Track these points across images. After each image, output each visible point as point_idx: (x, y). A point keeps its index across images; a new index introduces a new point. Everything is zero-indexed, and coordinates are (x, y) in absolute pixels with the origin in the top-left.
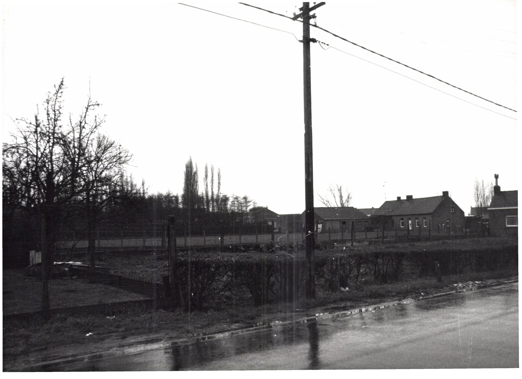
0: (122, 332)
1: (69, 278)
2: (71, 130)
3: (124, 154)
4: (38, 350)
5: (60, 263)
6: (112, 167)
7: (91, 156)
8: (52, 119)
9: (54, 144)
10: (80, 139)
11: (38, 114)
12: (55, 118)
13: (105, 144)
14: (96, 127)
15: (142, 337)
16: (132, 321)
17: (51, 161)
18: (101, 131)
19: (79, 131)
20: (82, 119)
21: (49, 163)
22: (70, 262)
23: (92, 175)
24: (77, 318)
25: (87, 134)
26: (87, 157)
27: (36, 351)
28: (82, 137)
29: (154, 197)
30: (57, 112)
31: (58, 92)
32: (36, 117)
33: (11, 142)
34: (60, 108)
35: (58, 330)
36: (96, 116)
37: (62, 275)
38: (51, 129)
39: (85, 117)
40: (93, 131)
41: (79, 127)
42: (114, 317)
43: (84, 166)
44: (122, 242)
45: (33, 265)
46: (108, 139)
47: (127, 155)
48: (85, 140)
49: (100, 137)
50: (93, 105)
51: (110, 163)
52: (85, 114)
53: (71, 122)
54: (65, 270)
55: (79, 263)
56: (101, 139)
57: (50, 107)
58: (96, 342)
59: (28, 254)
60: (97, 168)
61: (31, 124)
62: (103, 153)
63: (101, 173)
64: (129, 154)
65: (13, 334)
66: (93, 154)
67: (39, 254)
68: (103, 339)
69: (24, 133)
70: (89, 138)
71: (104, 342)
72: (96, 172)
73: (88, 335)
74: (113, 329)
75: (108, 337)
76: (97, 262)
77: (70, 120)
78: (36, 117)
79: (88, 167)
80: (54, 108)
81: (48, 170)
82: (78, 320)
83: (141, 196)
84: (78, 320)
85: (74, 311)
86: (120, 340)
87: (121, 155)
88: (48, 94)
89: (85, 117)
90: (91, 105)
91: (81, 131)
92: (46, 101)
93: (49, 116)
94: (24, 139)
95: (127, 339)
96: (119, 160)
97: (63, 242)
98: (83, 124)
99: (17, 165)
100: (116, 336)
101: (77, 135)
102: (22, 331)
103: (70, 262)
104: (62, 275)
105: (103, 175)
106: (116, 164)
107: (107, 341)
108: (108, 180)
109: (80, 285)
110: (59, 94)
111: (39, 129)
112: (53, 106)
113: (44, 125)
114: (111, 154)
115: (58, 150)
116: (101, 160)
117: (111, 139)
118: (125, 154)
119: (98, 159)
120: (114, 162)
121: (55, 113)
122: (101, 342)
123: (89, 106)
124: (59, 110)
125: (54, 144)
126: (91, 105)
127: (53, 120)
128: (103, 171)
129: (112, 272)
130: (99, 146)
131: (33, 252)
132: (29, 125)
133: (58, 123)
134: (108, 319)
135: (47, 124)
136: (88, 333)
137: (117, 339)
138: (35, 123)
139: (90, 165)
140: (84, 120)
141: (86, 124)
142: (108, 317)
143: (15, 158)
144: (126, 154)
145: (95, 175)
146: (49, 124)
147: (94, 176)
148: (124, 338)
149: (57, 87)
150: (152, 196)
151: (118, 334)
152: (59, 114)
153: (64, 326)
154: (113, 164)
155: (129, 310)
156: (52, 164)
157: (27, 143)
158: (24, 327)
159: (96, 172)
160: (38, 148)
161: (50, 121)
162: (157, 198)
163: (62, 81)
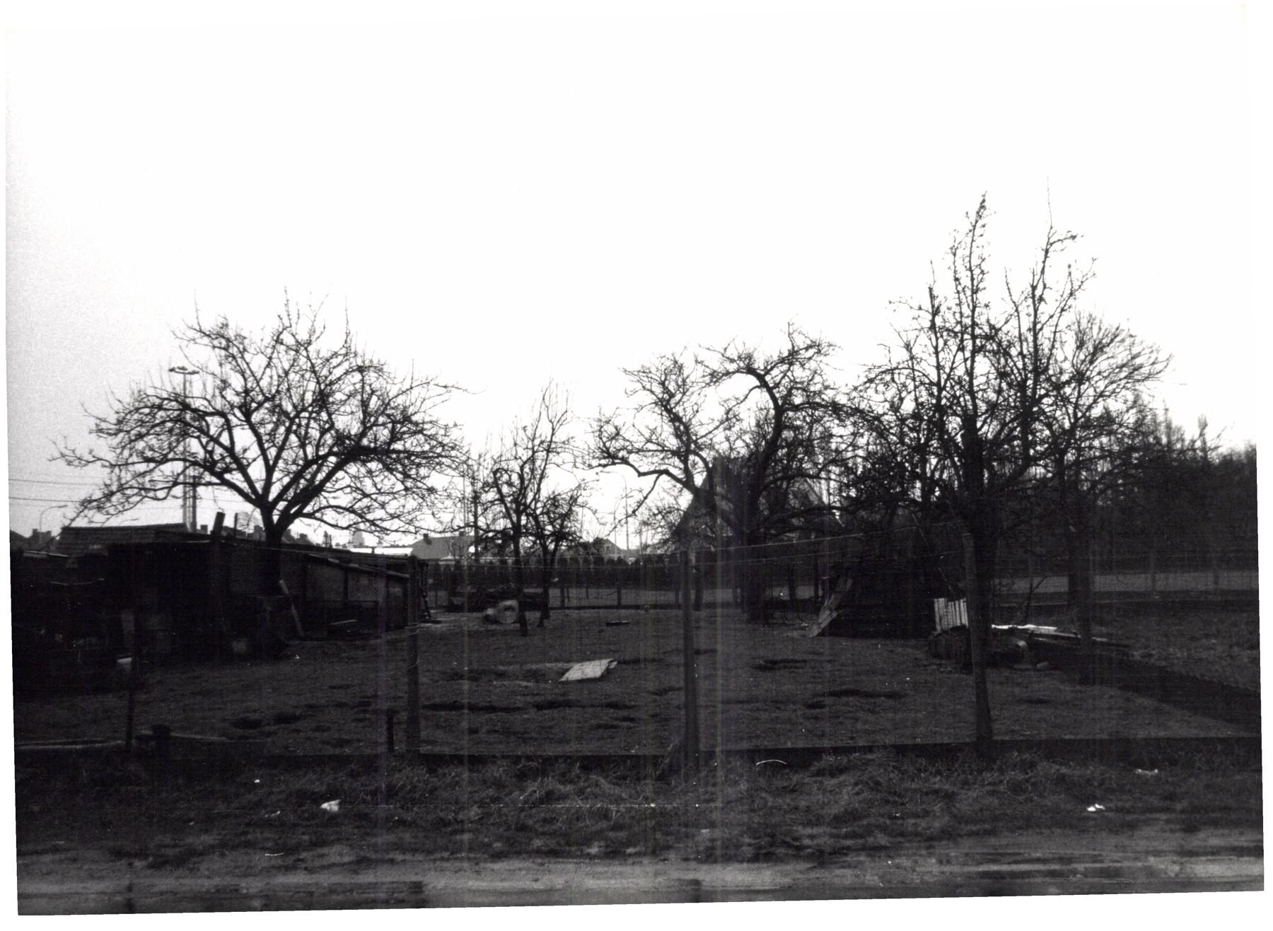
0: (1182, 812)
1: (1029, 666)
2: (1013, 312)
3: (1147, 357)
4: (977, 834)
5: (1006, 627)
6: (1117, 390)
7: (1061, 373)
8: (966, 289)
9: (975, 351)
10: (1035, 330)
11: (935, 282)
12: (973, 285)
13: (1095, 337)
14: (1071, 294)
15: (1241, 834)
16: (1207, 786)
17: (971, 393)
18: (1083, 305)
19: (1031, 311)
20: (1037, 278)
21: (968, 397)
22: (1030, 626)
23: (1068, 415)
24: (1061, 764)
25: (1051, 317)
26: (1052, 376)
27: (971, 834)
28: (1039, 326)
29: (1234, 458)
30: (976, 272)
31: (974, 227)
32: (931, 289)
33: (883, 362)
34: (983, 260)
35: (1017, 788)
36: (1069, 266)
37: (1013, 657)
38: (965, 315)
39: (1043, 272)
40: (1065, 305)
41: (1030, 301)
42: (1156, 771)
43: (1047, 395)
44: (1154, 581)
45: (944, 632)
46: (1101, 322)
47: (1157, 358)
48: (1047, 333)
49: (1081, 321)
50: (1059, 240)
51: (1112, 383)
52: (1042, 265)
53: (1009, 289)
54: (1018, 646)
55: (1050, 629)
56: (1084, 324)
57: (959, 263)
58: (1117, 833)
59: (931, 607)
60: (1080, 396)
61: (920, 308)
62: (1091, 362)
63: (1090, 408)
64: (1162, 357)
65: (918, 786)
66: (1067, 366)
67: (955, 605)
68: (1132, 826)
69: (903, 334)
70: (1057, 325)
71: (1137, 833)
72: (1076, 406)
73: (1091, 809)
74: (1155, 801)
75: (1147, 823)
76: (1096, 629)
77: (1007, 284)
78: (931, 289)
79: (1056, 397)
80: (970, 261)
81: (965, 409)
82: (1064, 770)
83: (1195, 458)
84: (1064, 770)
85: (1056, 749)
86: (1178, 835)
87: (1138, 361)
88: (954, 234)
89: (1043, 272)
90: (1054, 242)
91: (1036, 310)
92: (950, 251)
93: (960, 284)
94: (905, 350)
95: (1201, 835)
96: (1132, 371)
97: (1005, 581)
98: (1038, 293)
99: (895, 408)
100: (1168, 821)
101: (1026, 323)
102: (937, 782)
103: (1030, 626)
104: (1013, 657)
105: (1097, 412)
106: (1128, 383)
107: (1147, 831)
108: (1107, 423)
109: (1046, 684)
110: (978, 231)
111: (938, 321)
112: (967, 259)
113: (949, 309)
114: (1112, 361)
115: (983, 365)
116: (1089, 379)
117: (1109, 323)
118: (1150, 358)
119: (1080, 378)
120: (1120, 380)
121: (972, 275)
122: (1130, 833)
123: (1051, 244)
124: (980, 265)
125: (975, 351)
126: (1054, 242)
127: (969, 293)
128: (1095, 402)
129: (1137, 655)
130: (1081, 345)
131: (942, 600)
132: (916, 313)
133: (982, 297)
134: (1139, 776)
135: (957, 305)
136: (1093, 804)
137: (1172, 831)
138: (930, 306)
139: (1059, 393)
140: (1041, 280)
141: (1046, 290)
142: (1140, 771)
143: (889, 395)
144: (1154, 356)
145: (1075, 414)
146: (960, 304)
147: (1071, 416)
148: (1191, 829)
149: (973, 217)
150: (1231, 455)
151: (1173, 816)
152: (981, 276)
153: (1033, 780)
154: (1119, 385)
155: (1197, 758)
156: (974, 398)
157: (912, 358)
158: (939, 773)
159: (1076, 406)
160: (939, 367)
161: (962, 295)
162: (1245, 461)
163: (984, 201)
